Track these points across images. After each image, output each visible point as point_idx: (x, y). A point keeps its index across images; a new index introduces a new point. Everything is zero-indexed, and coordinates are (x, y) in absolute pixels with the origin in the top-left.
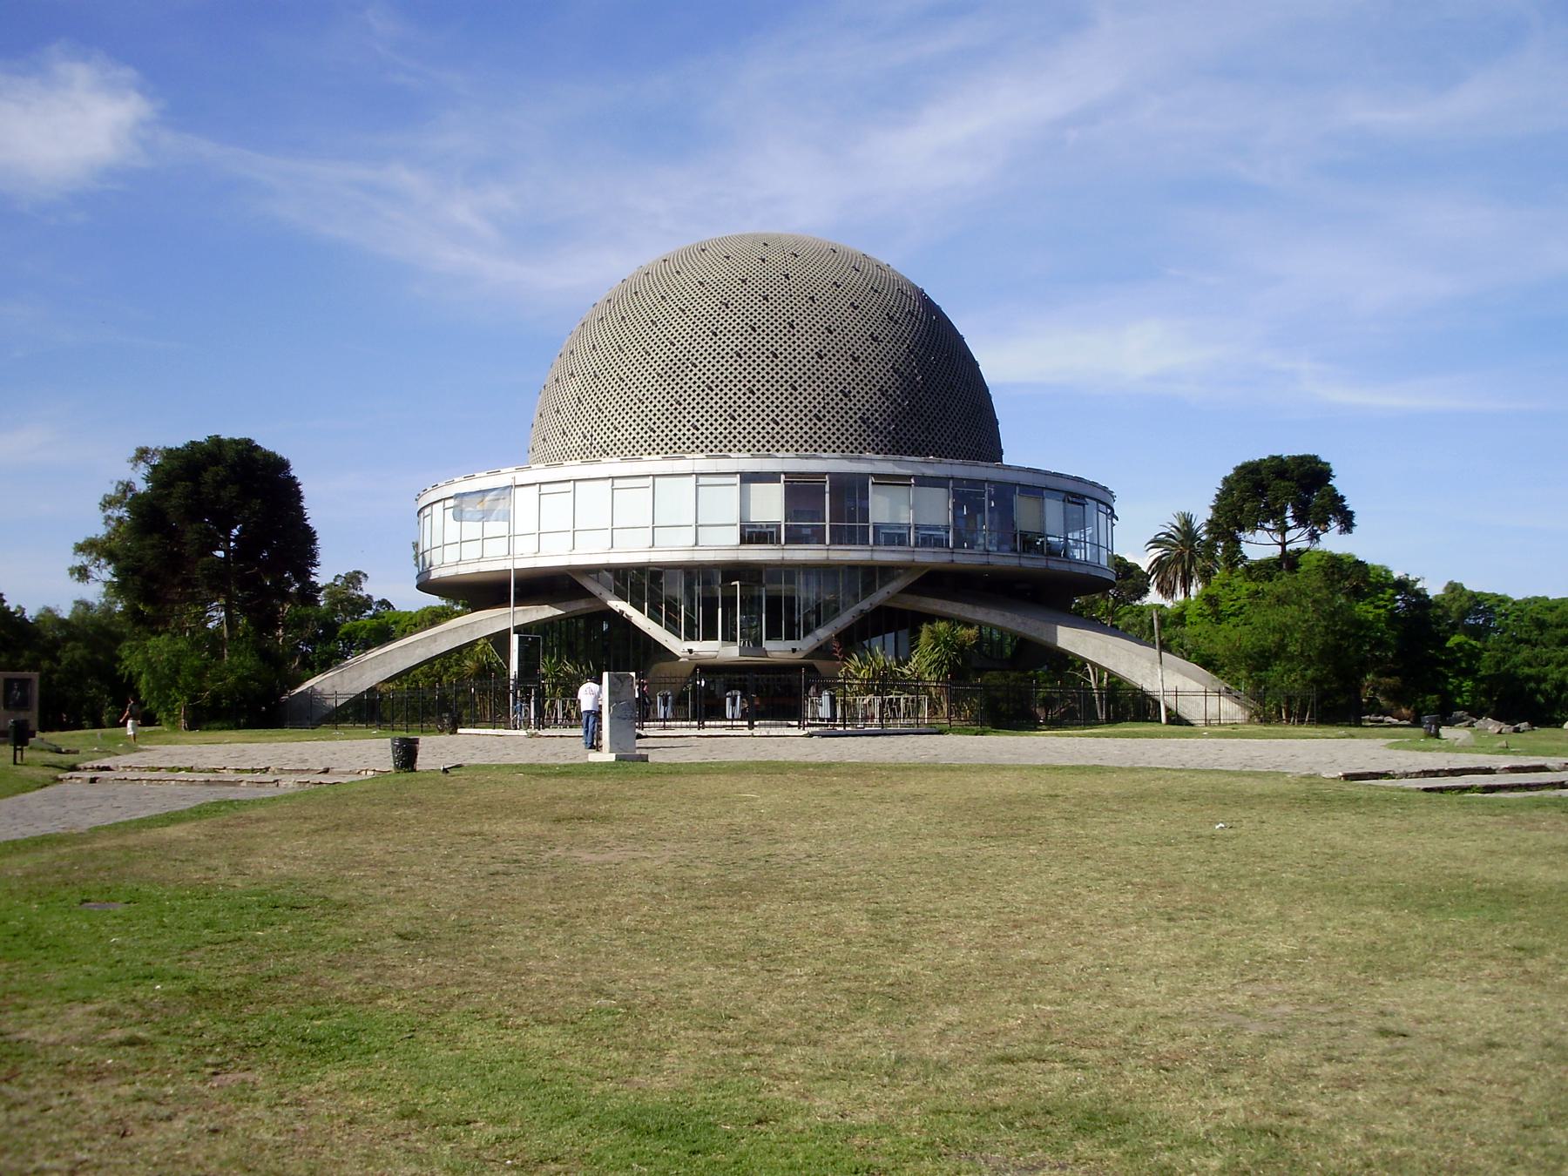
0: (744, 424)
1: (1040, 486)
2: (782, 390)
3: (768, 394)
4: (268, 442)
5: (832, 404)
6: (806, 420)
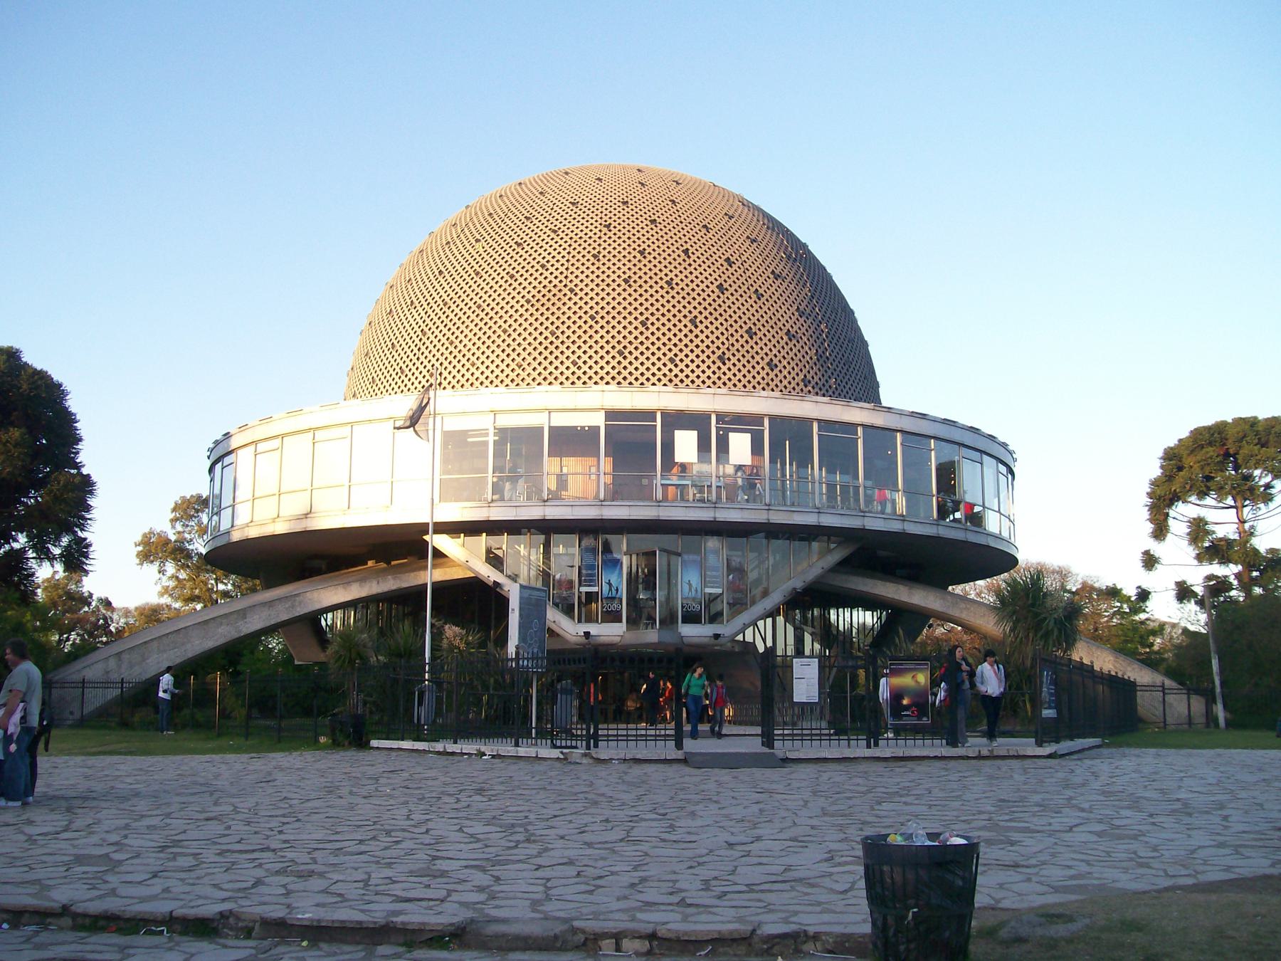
0: (636, 364)
1: (924, 433)
2: (680, 326)
3: (675, 330)
4: (57, 376)
5: (737, 346)
6: (709, 362)
